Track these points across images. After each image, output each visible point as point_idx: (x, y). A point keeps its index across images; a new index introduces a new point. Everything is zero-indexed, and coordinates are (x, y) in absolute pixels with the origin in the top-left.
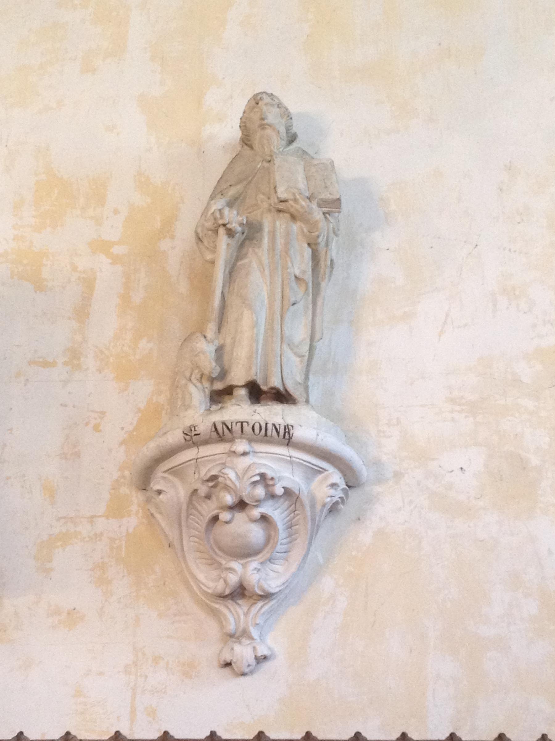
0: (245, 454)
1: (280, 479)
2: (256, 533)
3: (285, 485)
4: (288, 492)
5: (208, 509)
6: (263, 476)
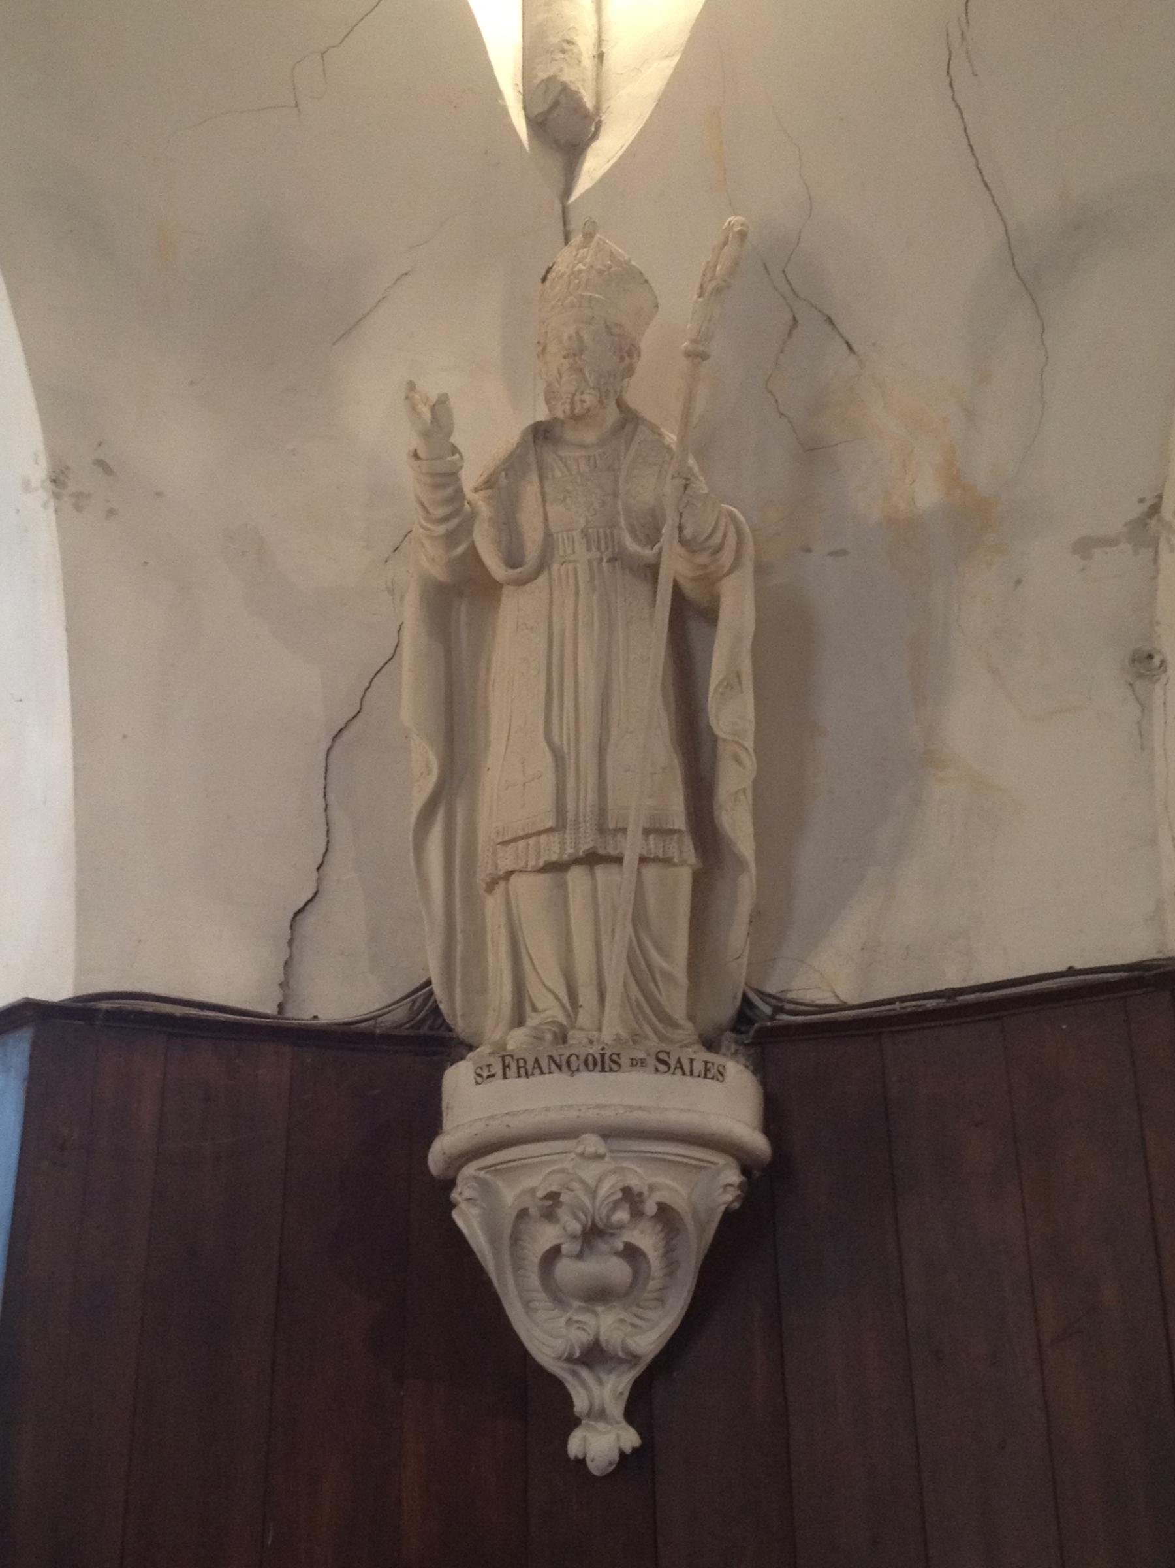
0: (598, 1157)
1: (652, 1188)
2: (617, 1270)
3: (659, 1200)
4: (664, 1211)
5: (546, 1236)
6: (627, 1191)
